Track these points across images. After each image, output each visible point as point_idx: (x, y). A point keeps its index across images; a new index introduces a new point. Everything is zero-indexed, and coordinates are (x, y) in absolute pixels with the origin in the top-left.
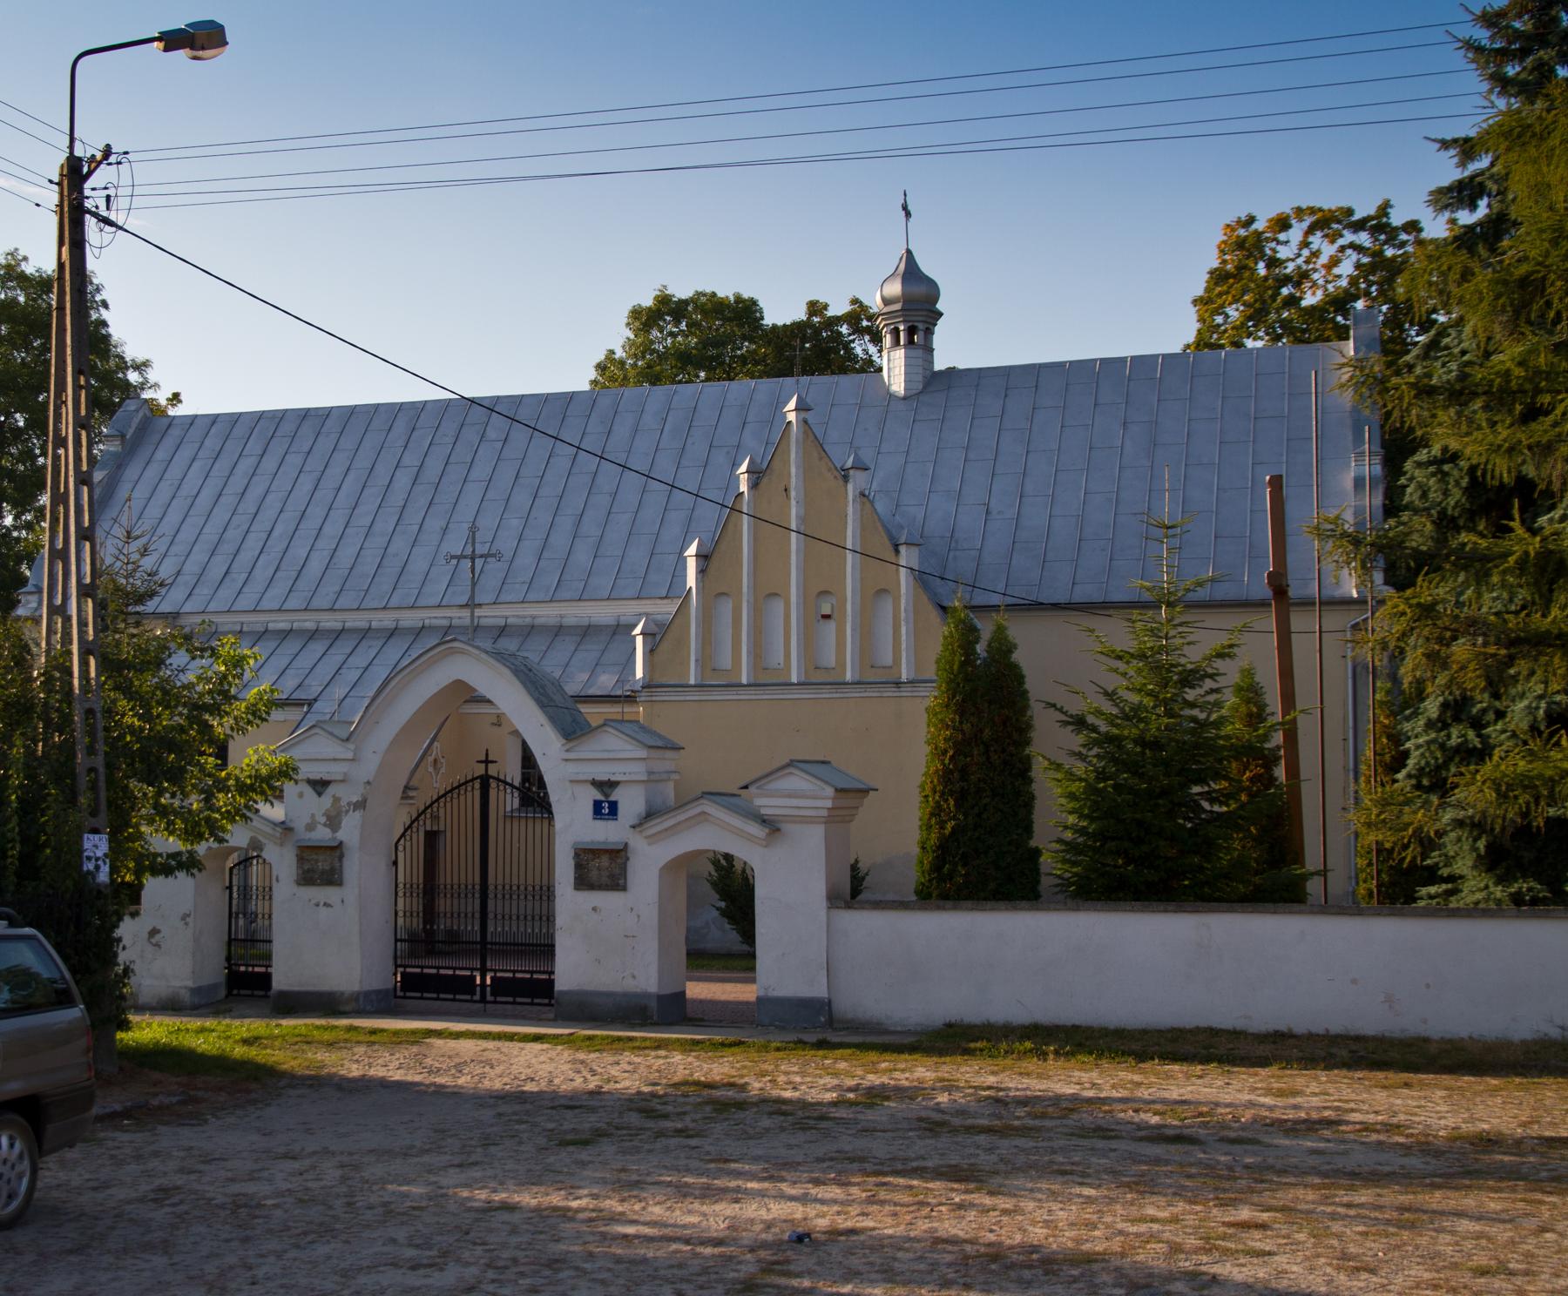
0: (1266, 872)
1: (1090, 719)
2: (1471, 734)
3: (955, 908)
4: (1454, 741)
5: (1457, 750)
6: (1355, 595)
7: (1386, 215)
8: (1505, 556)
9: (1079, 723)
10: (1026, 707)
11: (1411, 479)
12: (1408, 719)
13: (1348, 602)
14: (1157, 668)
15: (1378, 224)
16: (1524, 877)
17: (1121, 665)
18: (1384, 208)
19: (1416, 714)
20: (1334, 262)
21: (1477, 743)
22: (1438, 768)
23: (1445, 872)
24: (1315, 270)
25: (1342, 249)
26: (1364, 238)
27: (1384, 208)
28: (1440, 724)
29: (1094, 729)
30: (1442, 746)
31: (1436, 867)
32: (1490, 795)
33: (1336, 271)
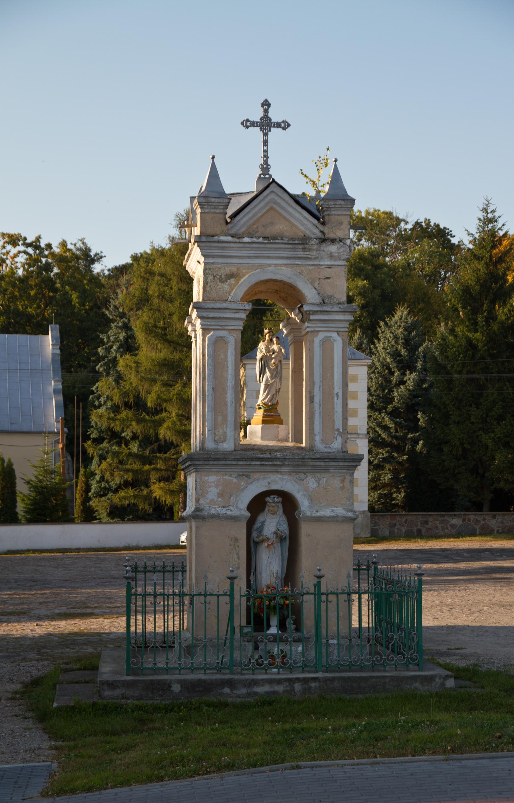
0: (66, 518)
1: (31, 482)
2: (106, 484)
3: (10, 525)
4: (103, 486)
5: (103, 488)
6: (56, 431)
7: (39, 241)
8: (122, 453)
9: (28, 483)
10: (15, 479)
11: (93, 420)
12: (92, 480)
13: (55, 433)
14: (45, 471)
15: (35, 245)
16: (117, 518)
17: (36, 469)
18: (38, 239)
19: (93, 479)
20: (16, 256)
21: (108, 486)
22: (99, 492)
23: (98, 517)
24: (7, 259)
25: (19, 252)
26: (30, 250)
27: (38, 239)
28: (99, 482)
29: (32, 484)
30: (100, 487)
31: (96, 516)
32: (118, 500)
33: (16, 259)
